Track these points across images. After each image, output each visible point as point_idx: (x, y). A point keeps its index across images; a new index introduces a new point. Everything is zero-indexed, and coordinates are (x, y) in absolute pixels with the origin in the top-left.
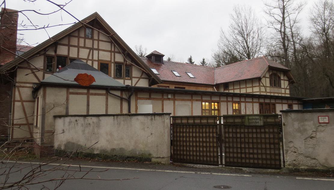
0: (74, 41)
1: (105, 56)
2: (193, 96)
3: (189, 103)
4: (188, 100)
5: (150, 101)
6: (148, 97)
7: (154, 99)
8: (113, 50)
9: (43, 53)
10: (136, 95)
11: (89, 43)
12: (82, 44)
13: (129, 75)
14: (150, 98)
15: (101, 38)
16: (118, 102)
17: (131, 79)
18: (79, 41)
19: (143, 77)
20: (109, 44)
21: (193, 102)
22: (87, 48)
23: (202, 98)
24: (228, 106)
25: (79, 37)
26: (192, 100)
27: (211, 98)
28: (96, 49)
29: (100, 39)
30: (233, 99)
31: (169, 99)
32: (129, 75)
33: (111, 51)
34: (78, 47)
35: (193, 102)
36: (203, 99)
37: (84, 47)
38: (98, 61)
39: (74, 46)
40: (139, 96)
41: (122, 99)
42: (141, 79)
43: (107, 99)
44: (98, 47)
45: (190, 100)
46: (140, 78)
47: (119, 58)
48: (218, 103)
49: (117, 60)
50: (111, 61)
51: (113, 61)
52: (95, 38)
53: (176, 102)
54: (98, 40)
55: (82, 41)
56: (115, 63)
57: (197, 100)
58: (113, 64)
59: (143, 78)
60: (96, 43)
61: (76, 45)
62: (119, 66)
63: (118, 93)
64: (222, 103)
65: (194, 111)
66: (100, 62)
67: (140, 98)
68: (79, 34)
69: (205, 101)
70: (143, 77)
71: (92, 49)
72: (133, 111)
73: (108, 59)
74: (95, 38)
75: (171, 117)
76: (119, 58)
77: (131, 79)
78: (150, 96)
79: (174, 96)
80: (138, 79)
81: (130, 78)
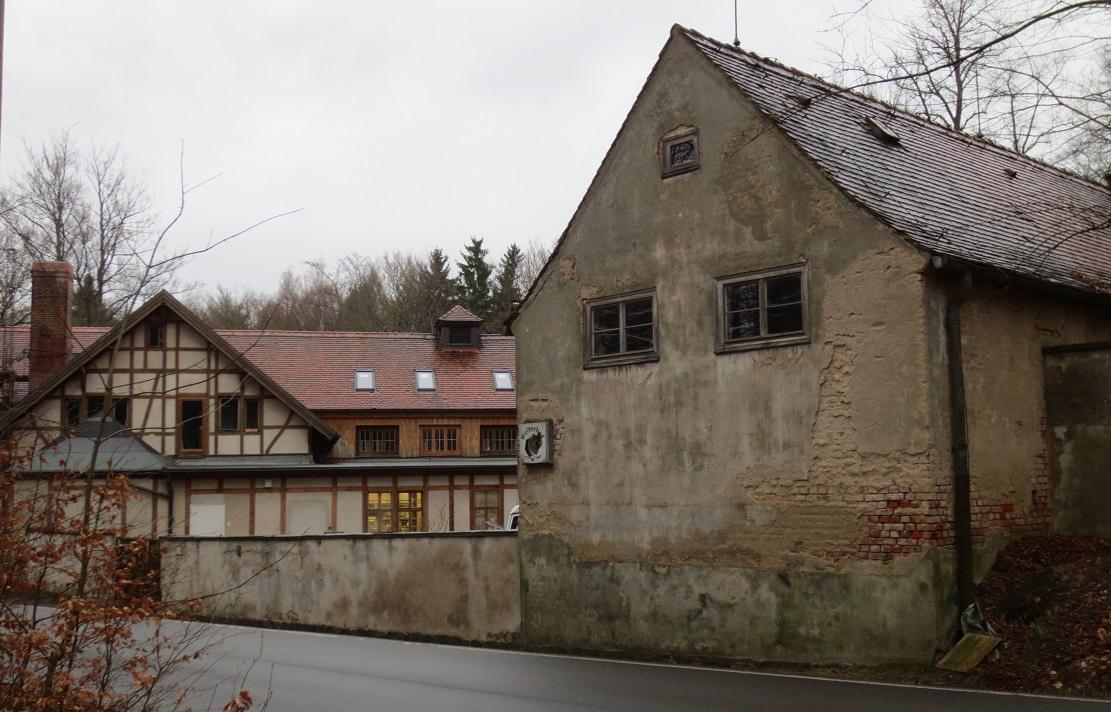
0: (122, 360)
1: (194, 384)
2: (288, 480)
3: (327, 497)
4: (323, 490)
5: (220, 496)
6: (216, 487)
7: (229, 491)
8: (213, 367)
9: (58, 393)
10: (188, 485)
11: (155, 358)
12: (139, 365)
13: (254, 422)
14: (220, 490)
15: (183, 344)
16: (147, 501)
17: (260, 433)
18: (132, 359)
19: (291, 424)
20: (203, 355)
21: (339, 493)
22: (152, 371)
23: (365, 483)
24: (455, 498)
25: (132, 350)
26: (334, 489)
27: (395, 482)
28: (172, 372)
29: (182, 345)
30: (472, 481)
31: (269, 490)
32: (254, 422)
33: (207, 371)
34: (132, 371)
35: (339, 493)
36: (476, 483)
37: (145, 370)
38: (177, 397)
39: (123, 371)
40: (193, 487)
41: (155, 496)
42: (287, 431)
43: (283, 499)
44: (145, 363)
45: (330, 490)
46: (283, 428)
47: (228, 384)
48: (422, 492)
49: (221, 390)
50: (207, 395)
51: (212, 393)
52: (168, 346)
53: (290, 497)
54: (177, 349)
55: (139, 356)
56: (219, 397)
57: (350, 489)
58: (212, 401)
59: (293, 427)
60: (171, 355)
61: (127, 367)
62: (228, 405)
63: (148, 485)
64: (430, 493)
65: (257, 527)
66: (180, 398)
67: (197, 492)
68: (132, 343)
69: (379, 491)
70: (291, 424)
71: (162, 372)
72: (179, 532)
73: (201, 389)
74: (168, 346)
75: (118, 538)
76: (228, 384)
77: (260, 433)
78: (221, 484)
79: (284, 483)
80: (278, 431)
81: (256, 430)
